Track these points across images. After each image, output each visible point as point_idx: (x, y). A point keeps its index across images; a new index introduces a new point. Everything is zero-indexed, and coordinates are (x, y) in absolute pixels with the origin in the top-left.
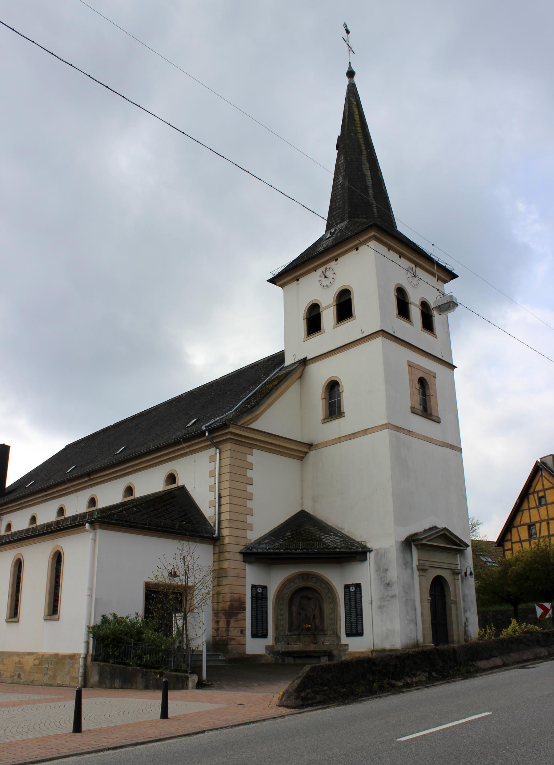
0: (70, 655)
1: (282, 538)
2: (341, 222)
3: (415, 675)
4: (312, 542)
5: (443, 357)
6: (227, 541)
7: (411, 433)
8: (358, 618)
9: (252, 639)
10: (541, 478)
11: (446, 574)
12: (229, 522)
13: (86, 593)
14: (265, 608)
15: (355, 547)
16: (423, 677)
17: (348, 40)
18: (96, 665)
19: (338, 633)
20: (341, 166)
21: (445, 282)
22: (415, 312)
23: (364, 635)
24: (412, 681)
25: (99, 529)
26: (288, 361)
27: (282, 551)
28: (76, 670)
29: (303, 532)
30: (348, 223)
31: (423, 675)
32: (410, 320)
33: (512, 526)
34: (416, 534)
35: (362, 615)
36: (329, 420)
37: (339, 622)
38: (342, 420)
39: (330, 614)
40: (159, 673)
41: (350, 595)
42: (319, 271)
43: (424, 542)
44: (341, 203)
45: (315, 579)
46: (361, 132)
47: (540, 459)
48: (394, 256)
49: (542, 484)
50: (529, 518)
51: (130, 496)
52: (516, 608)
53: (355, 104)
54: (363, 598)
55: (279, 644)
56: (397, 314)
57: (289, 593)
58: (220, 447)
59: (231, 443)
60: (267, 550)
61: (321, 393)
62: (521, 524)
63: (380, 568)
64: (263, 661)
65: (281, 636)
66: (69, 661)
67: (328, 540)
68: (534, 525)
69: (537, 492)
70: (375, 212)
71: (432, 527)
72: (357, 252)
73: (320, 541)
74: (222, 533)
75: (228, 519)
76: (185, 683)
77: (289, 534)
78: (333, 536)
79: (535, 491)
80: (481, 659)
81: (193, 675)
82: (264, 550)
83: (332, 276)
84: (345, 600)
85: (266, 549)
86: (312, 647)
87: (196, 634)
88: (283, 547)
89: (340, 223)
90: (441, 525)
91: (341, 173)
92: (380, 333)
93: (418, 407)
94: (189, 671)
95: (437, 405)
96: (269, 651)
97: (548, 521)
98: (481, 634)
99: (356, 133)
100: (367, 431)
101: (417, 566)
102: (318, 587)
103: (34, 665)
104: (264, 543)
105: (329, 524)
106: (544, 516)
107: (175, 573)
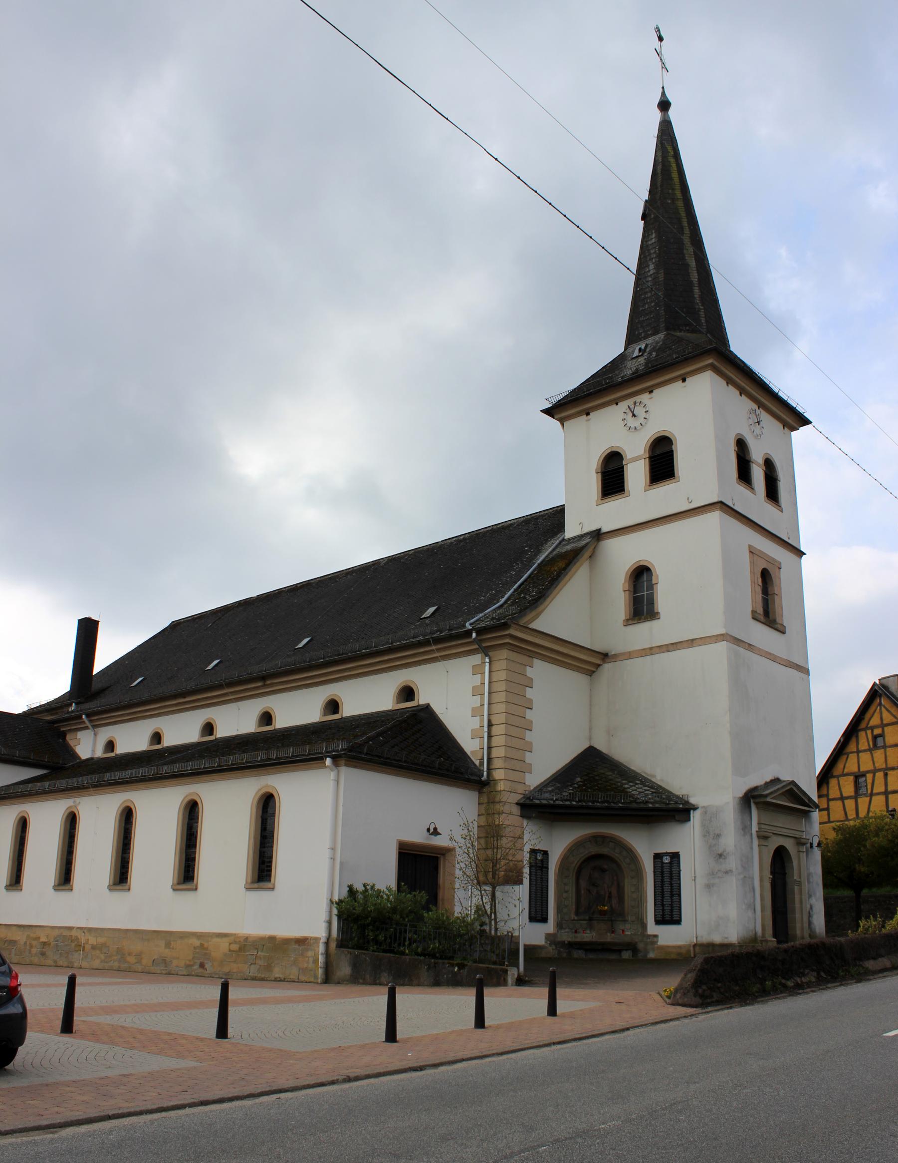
0: (297, 938)
1: (570, 785)
2: (654, 334)
3: (803, 975)
4: (612, 793)
5: (789, 539)
6: (501, 786)
7: (752, 647)
8: (674, 900)
9: (530, 923)
10: (879, 708)
11: (789, 844)
12: (505, 761)
13: (327, 854)
14: (546, 882)
15: (673, 802)
16: (811, 977)
17: (661, 52)
18: (346, 952)
19: (643, 920)
20: (651, 247)
21: (794, 429)
22: (758, 474)
23: (682, 923)
24: (802, 981)
25: (345, 766)
26: (572, 529)
27: (574, 803)
28: (309, 960)
29: (597, 778)
30: (666, 338)
31: (812, 975)
32: (752, 486)
33: (830, 776)
34: (755, 788)
35: (679, 895)
36: (636, 622)
37: (645, 905)
38: (654, 623)
39: (633, 892)
40: (457, 965)
41: (662, 867)
42: (624, 405)
43: (769, 799)
44: (653, 304)
45: (613, 844)
46: (680, 199)
47: (879, 680)
48: (733, 392)
49: (879, 716)
50: (857, 765)
51: (331, 714)
52: (858, 895)
53: (672, 153)
54: (681, 872)
55: (563, 931)
56: (737, 478)
57: (576, 862)
58: (490, 654)
59: (507, 649)
60: (554, 801)
61: (623, 582)
62: (844, 772)
63: (708, 833)
64: (543, 954)
65: (566, 921)
66: (297, 946)
67: (635, 791)
68: (863, 775)
69: (872, 728)
70: (703, 323)
71: (773, 778)
72: (684, 384)
73: (624, 791)
74: (493, 775)
75: (504, 756)
76: (502, 979)
77: (579, 779)
78: (639, 785)
79: (869, 726)
80: (868, 959)
81: (512, 968)
82: (550, 801)
83: (644, 415)
84: (654, 875)
85: (552, 800)
86: (609, 938)
87: (508, 915)
88: (576, 798)
89: (651, 334)
90: (786, 777)
91: (652, 259)
92: (717, 505)
93: (760, 610)
94: (506, 963)
95: (782, 608)
96: (550, 941)
97: (886, 771)
98: (866, 927)
99: (674, 200)
100: (695, 641)
101: (757, 832)
102: (617, 855)
103: (230, 950)
104: (547, 792)
105: (633, 768)
106: (880, 764)
107: (435, 829)
